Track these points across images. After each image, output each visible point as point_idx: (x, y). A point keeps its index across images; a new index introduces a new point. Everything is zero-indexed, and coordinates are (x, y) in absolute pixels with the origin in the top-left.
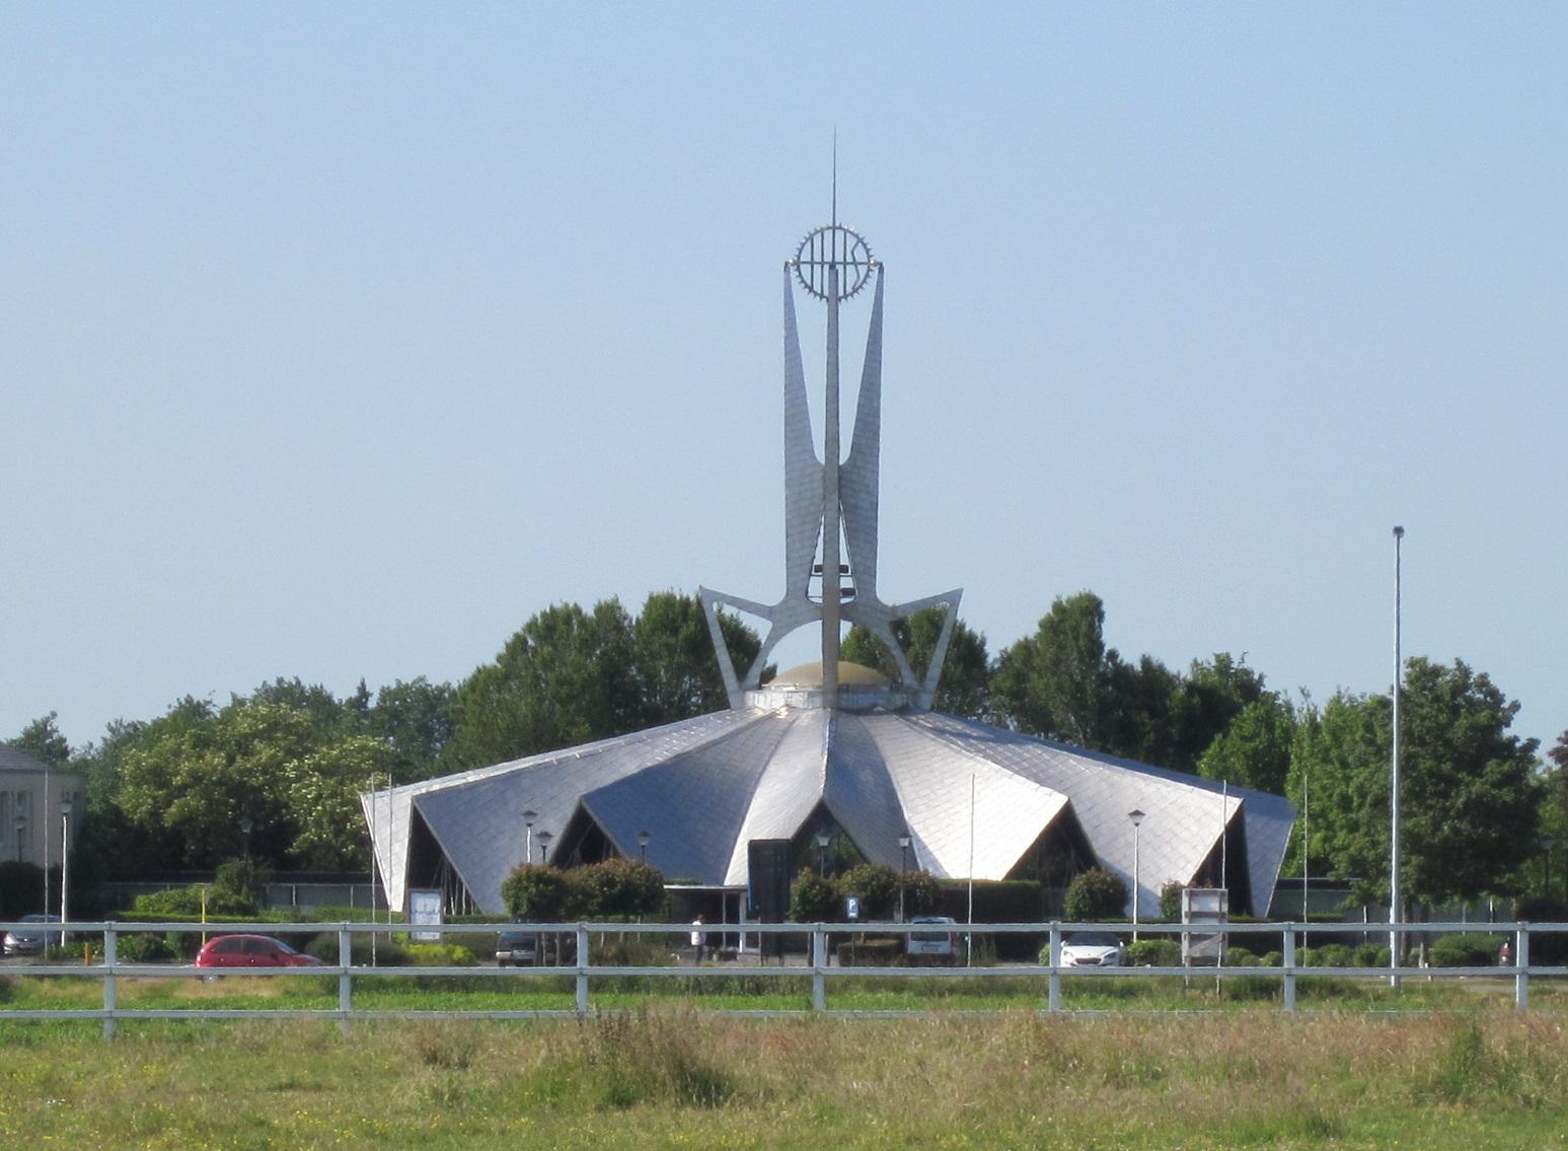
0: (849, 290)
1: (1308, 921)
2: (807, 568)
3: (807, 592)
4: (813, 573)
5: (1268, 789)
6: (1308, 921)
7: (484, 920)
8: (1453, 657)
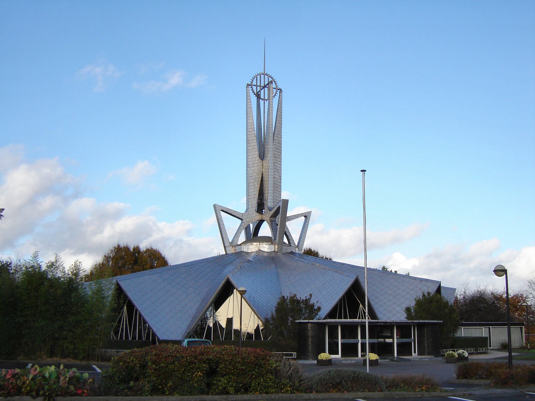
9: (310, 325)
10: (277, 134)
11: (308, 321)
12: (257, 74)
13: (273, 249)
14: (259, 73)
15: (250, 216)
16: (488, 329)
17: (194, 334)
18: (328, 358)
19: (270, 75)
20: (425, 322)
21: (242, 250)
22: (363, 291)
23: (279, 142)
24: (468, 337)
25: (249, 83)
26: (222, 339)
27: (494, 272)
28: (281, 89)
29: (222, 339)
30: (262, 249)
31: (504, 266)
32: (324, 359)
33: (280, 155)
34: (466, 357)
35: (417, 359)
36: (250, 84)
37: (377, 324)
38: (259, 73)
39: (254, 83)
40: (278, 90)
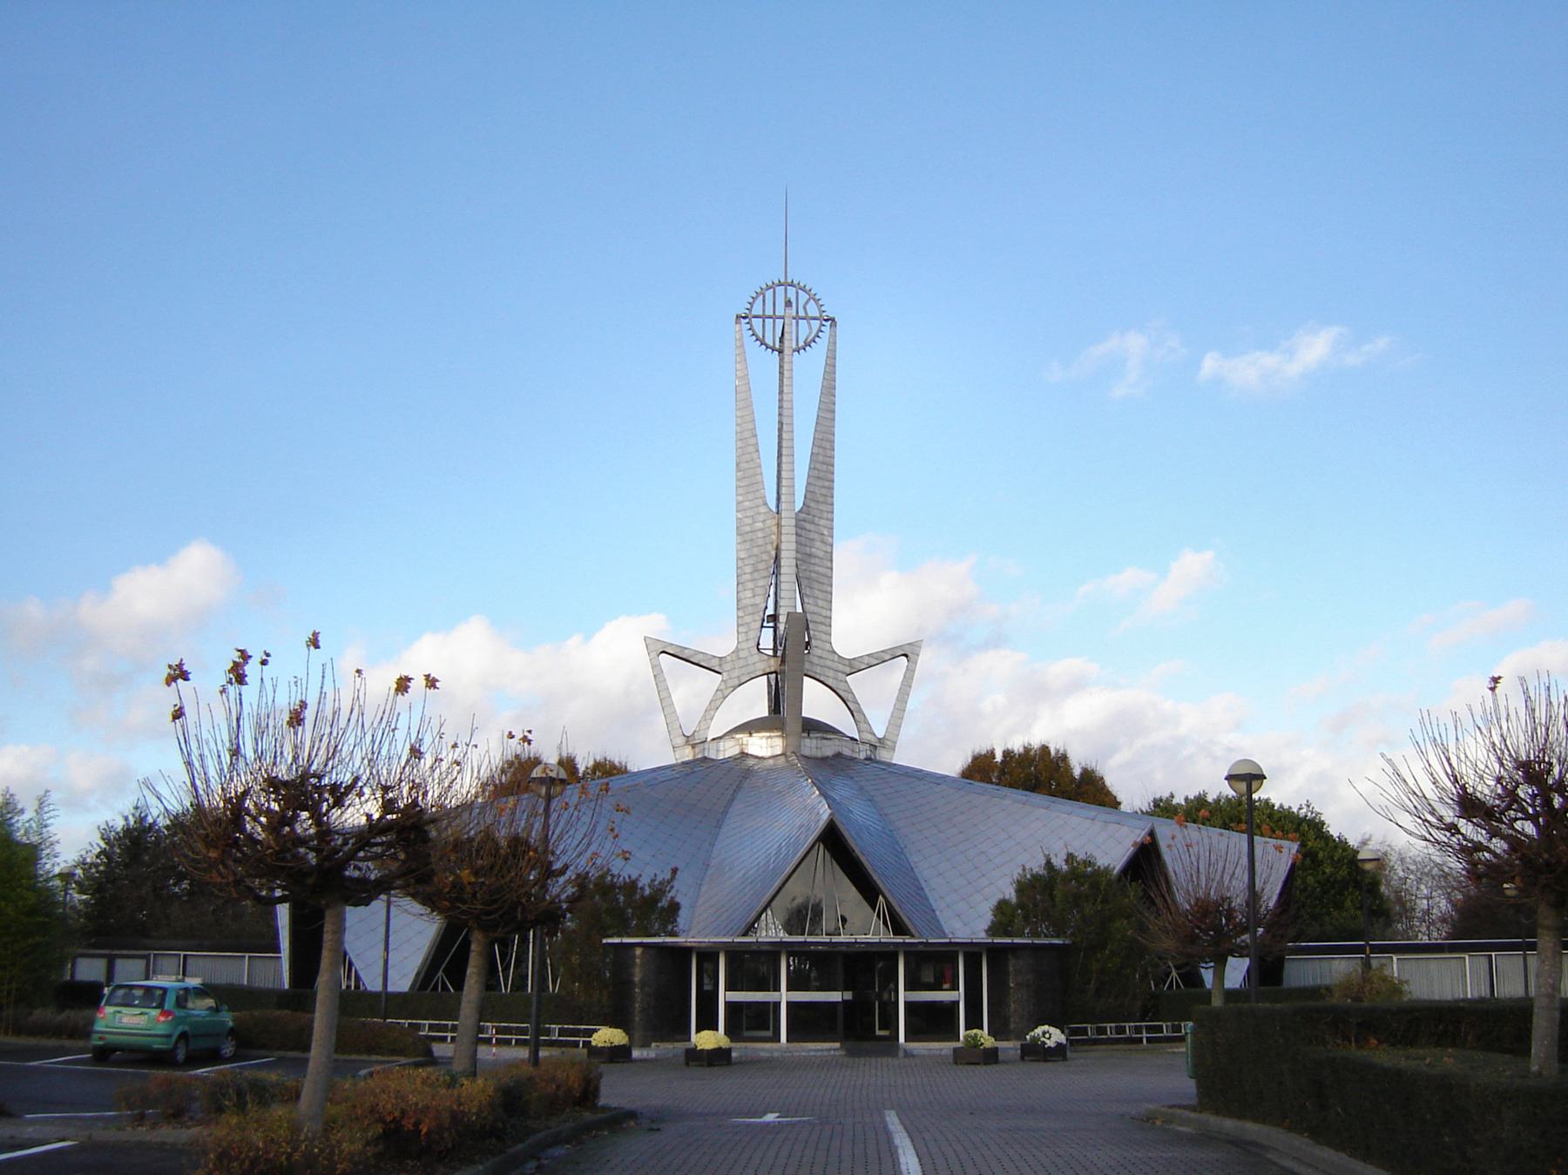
0: (801, 344)
1: (826, 935)
2: (758, 617)
3: (758, 644)
4: (765, 624)
5: (79, 871)
6: (826, 935)
7: (1236, 1142)
8: (1170, 791)
9: (638, 951)
10: (822, 440)
11: (731, 941)
12: (764, 287)
13: (778, 748)
14: (770, 284)
15: (742, 663)
16: (1484, 962)
17: (446, 980)
18: (611, 1040)
19: (802, 285)
20: (1016, 943)
21: (706, 755)
22: (854, 854)
23: (827, 460)
24: (290, 974)
25: (743, 312)
26: (554, 990)
27: (1226, 782)
28: (833, 320)
29: (554, 990)
30: (752, 750)
31: (1242, 758)
32: (599, 1045)
33: (829, 494)
34: (1050, 1047)
35: (945, 1050)
36: (743, 315)
37: (807, 949)
38: (770, 284)
39: (757, 310)
40: (824, 323)
